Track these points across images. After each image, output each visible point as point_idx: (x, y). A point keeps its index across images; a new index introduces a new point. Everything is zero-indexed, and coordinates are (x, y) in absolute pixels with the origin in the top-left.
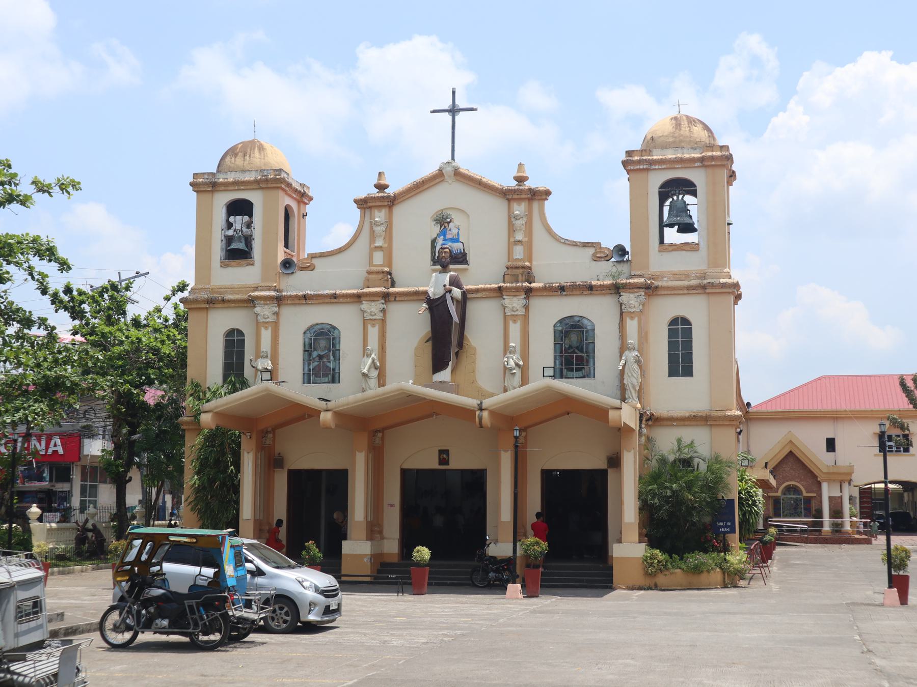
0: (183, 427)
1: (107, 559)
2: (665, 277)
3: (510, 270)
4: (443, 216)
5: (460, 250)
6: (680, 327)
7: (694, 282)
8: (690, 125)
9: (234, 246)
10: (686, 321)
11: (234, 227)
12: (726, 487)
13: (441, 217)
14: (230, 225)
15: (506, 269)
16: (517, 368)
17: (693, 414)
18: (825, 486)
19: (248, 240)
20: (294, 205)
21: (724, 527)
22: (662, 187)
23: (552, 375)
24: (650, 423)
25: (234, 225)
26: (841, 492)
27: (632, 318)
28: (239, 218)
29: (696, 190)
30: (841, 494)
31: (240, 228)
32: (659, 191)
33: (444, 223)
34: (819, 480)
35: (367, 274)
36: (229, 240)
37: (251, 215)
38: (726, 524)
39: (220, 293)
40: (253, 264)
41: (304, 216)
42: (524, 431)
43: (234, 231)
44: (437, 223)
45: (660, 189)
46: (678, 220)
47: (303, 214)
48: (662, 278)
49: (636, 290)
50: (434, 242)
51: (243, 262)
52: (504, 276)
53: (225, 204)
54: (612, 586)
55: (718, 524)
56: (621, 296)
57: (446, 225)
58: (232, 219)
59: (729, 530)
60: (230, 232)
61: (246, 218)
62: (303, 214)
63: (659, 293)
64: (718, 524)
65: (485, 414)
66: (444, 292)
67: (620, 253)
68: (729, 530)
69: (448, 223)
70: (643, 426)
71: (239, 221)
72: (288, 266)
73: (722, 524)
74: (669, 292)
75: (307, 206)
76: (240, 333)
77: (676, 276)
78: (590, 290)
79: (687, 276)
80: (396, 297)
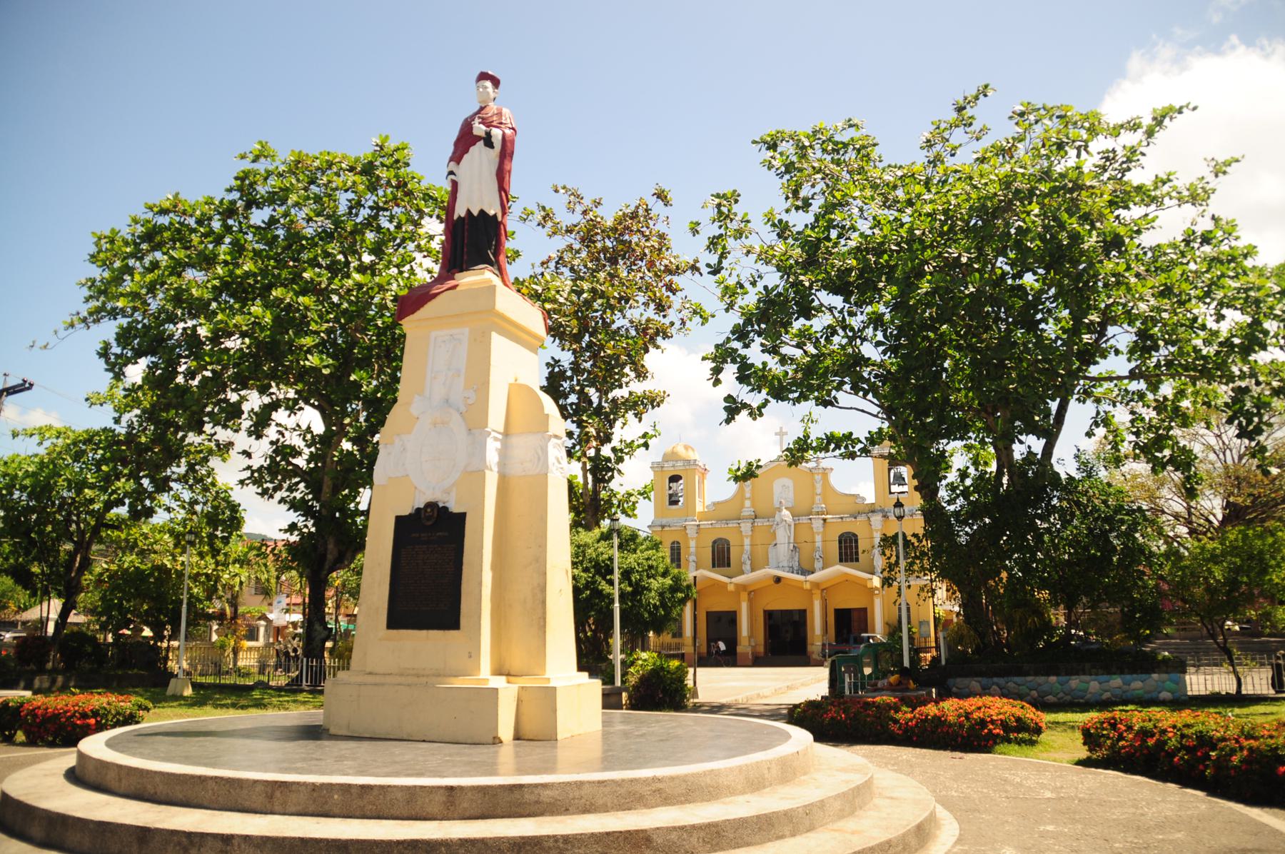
14: (670, 488)
36: (671, 496)
60: (671, 492)
76: (678, 543)
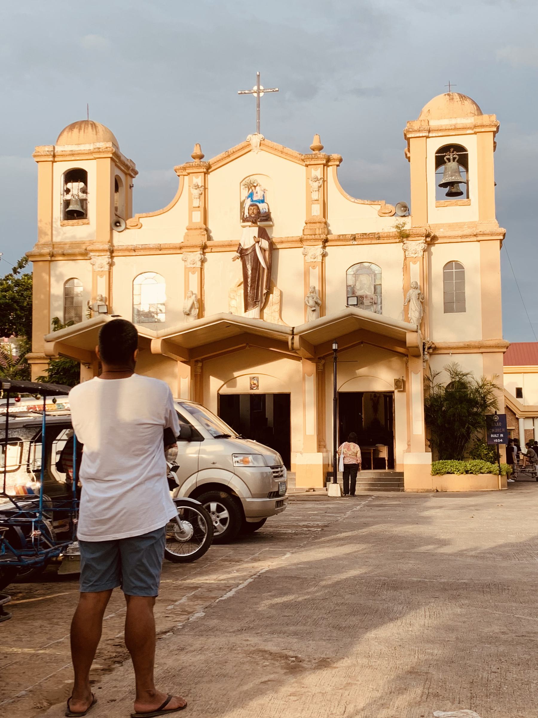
0: (29, 362)
1: (239, 618)
2: (442, 228)
3: (308, 225)
4: (251, 181)
5: (265, 209)
6: (454, 270)
7: (467, 232)
8: (462, 99)
9: (71, 208)
10: (459, 266)
11: (71, 193)
12: (494, 403)
13: (249, 182)
14: (68, 191)
15: (305, 225)
16: (317, 306)
17: (467, 344)
18: (521, 421)
19: (83, 202)
20: (122, 176)
21: (497, 438)
22: (438, 152)
23: (356, 303)
24: (431, 351)
25: (71, 190)
26: (534, 426)
27: (415, 263)
28: (75, 184)
29: (467, 154)
30: (534, 427)
31: (76, 193)
32: (436, 157)
33: (251, 187)
34: (517, 416)
35: (186, 231)
36: (67, 203)
37: (86, 183)
38: (499, 436)
39: (61, 248)
40: (88, 224)
41: (131, 187)
42: (323, 359)
43: (72, 195)
44: (246, 187)
45: (436, 153)
46: (453, 179)
47: (130, 185)
48: (439, 229)
49: (417, 238)
50: (242, 204)
51: (81, 221)
52: (303, 230)
53: (64, 173)
54: (404, 489)
55: (492, 436)
56: (404, 244)
57: (253, 188)
58: (69, 185)
59: (501, 440)
60: (68, 197)
61: (82, 185)
62: (130, 185)
63: (439, 241)
64: (492, 436)
65: (297, 338)
66: (254, 242)
67: (402, 209)
68: (501, 440)
69: (255, 187)
70: (426, 353)
71: (75, 187)
72: (118, 224)
73: (495, 436)
74: (446, 241)
75: (133, 179)
77: (451, 226)
78: (378, 240)
79: (460, 226)
80: (212, 249)
